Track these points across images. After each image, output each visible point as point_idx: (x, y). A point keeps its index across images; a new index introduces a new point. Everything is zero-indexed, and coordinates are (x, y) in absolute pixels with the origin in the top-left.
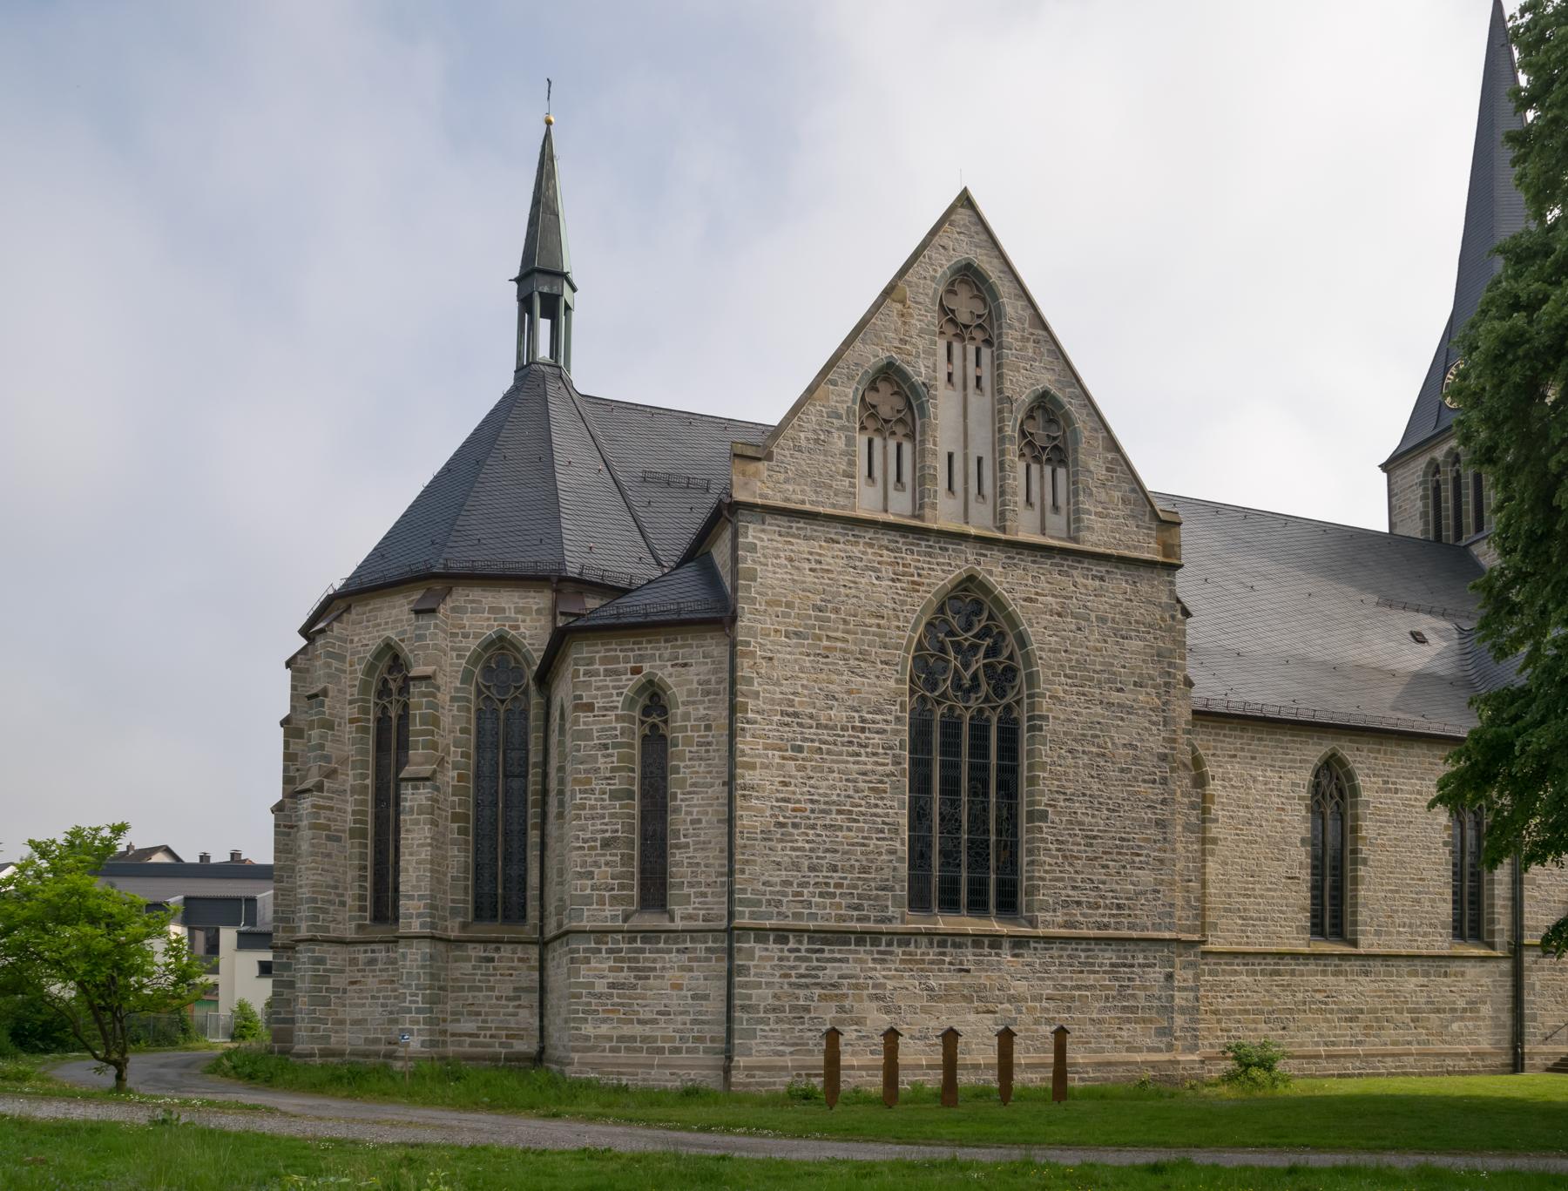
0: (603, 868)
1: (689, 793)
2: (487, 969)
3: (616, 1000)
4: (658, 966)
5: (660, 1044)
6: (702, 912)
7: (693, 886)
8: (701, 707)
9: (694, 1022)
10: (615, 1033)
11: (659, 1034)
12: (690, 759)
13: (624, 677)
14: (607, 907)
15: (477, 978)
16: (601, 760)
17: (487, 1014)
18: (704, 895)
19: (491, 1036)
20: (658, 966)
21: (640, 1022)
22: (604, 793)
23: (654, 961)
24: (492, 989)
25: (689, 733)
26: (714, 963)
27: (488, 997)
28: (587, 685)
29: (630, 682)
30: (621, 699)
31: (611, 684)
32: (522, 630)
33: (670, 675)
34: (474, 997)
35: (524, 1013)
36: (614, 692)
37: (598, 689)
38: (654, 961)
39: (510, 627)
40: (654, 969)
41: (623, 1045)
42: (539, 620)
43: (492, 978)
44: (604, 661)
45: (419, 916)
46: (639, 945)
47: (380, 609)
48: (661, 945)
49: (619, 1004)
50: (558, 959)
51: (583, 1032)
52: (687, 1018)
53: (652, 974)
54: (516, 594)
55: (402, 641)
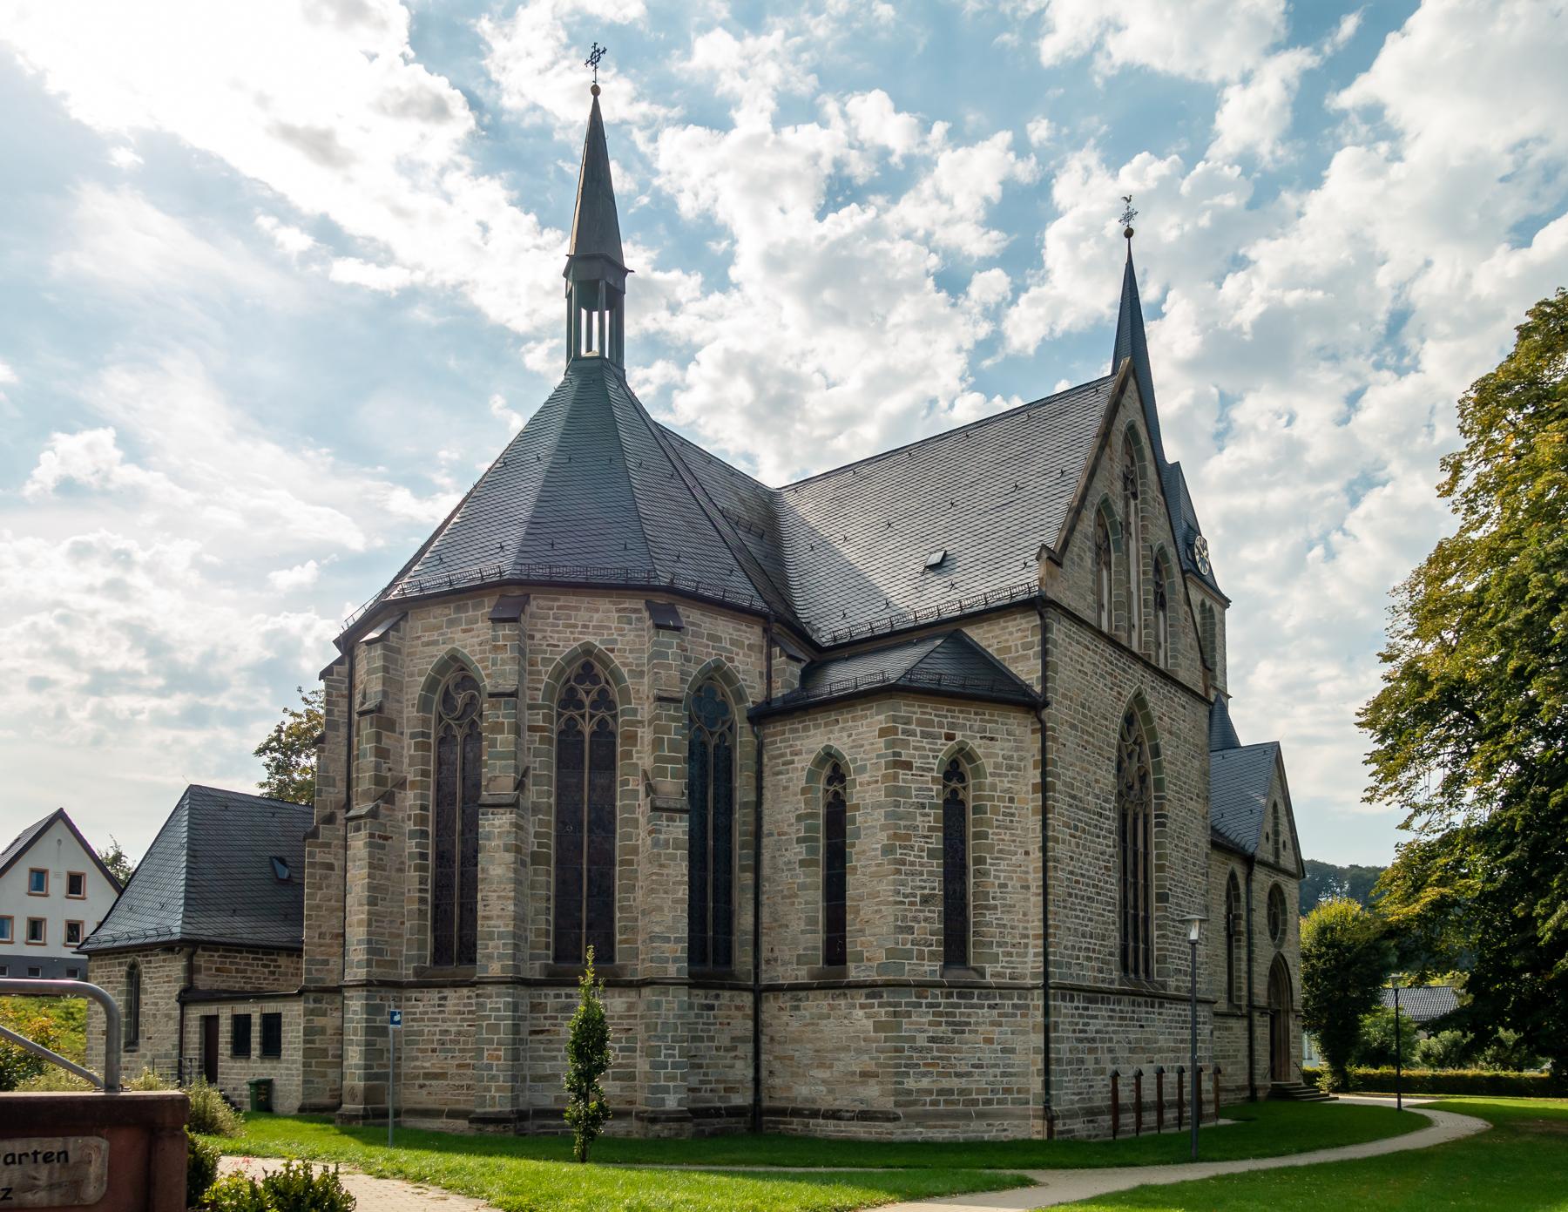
0: (923, 924)
1: (997, 858)
2: (708, 1018)
3: (936, 1054)
4: (972, 1020)
5: (974, 1096)
6: (1008, 971)
7: (1001, 946)
8: (1006, 780)
9: (1004, 1074)
10: (935, 1087)
11: (974, 1086)
12: (997, 827)
13: (939, 742)
14: (926, 962)
15: (700, 1027)
16: (919, 818)
17: (708, 1066)
18: (1010, 954)
19: (711, 1091)
20: (972, 1020)
21: (958, 1075)
22: (923, 851)
23: (969, 1015)
24: (711, 1039)
25: (996, 803)
26: (1019, 1018)
27: (710, 1048)
28: (906, 744)
29: (945, 747)
30: (937, 762)
31: (928, 746)
32: (736, 664)
33: (980, 746)
34: (696, 1048)
35: (739, 1064)
36: (931, 754)
37: (916, 748)
38: (969, 1015)
39: (727, 658)
40: (968, 1024)
41: (942, 1098)
42: (750, 656)
43: (712, 1027)
44: (920, 723)
45: (676, 960)
46: (955, 1000)
47: (577, 609)
48: (975, 1001)
49: (939, 1058)
50: (770, 1006)
51: (906, 1086)
52: (998, 1071)
53: (967, 1029)
54: (731, 625)
55: (612, 651)
